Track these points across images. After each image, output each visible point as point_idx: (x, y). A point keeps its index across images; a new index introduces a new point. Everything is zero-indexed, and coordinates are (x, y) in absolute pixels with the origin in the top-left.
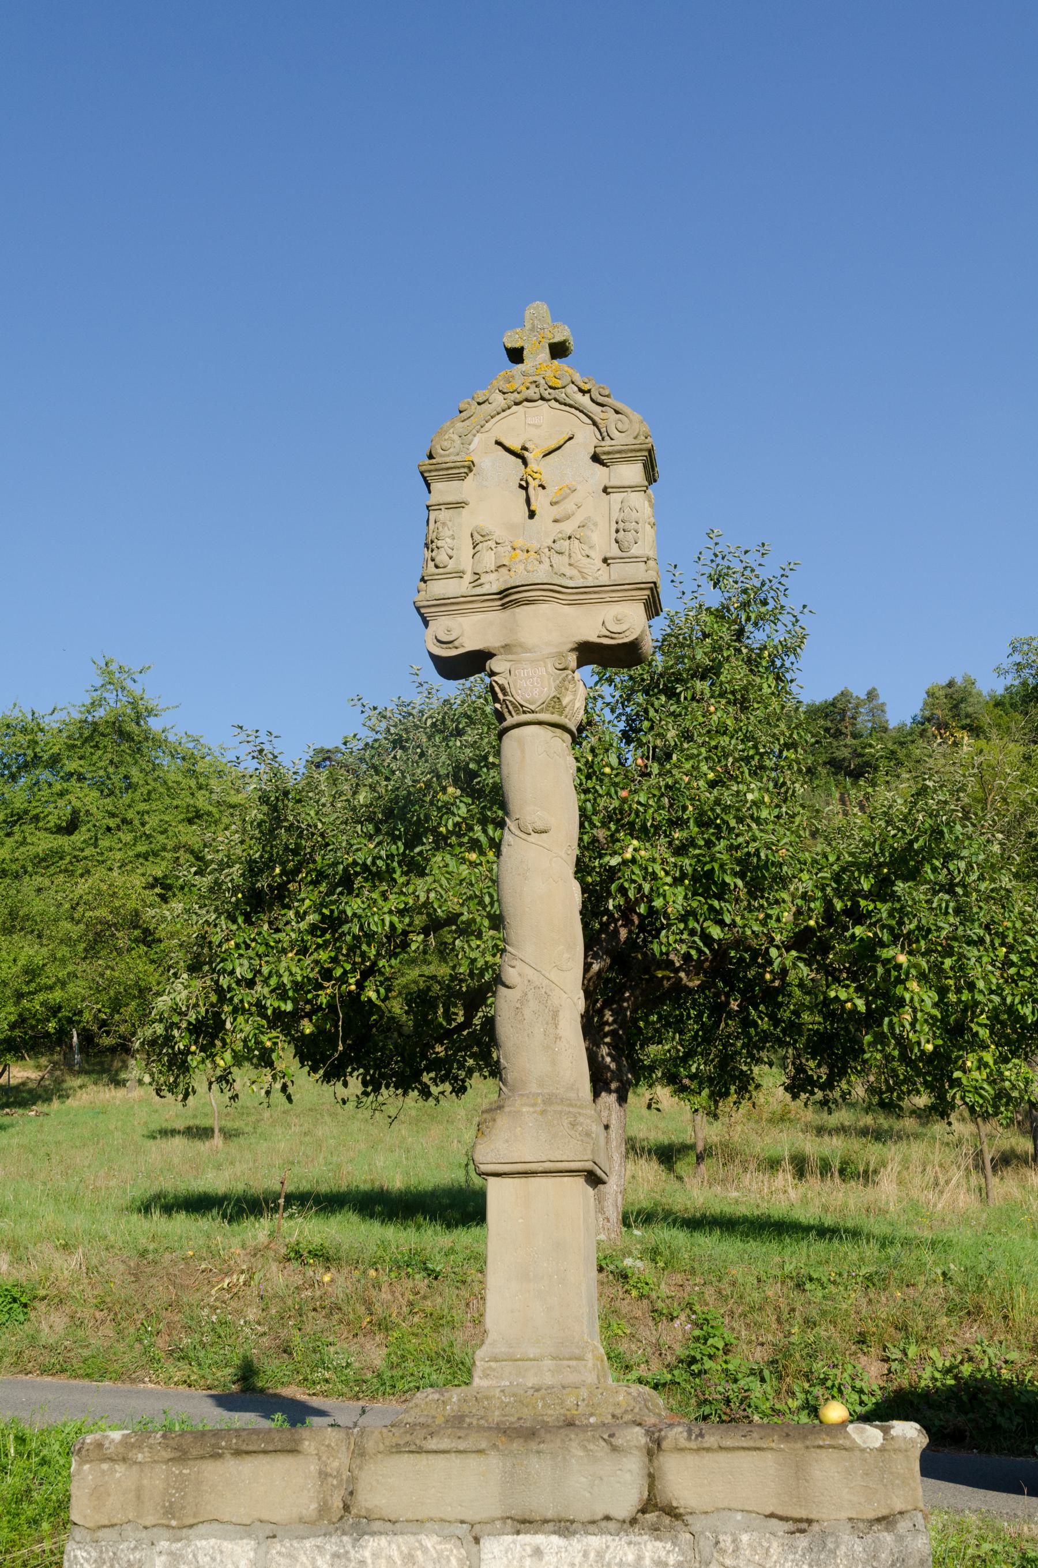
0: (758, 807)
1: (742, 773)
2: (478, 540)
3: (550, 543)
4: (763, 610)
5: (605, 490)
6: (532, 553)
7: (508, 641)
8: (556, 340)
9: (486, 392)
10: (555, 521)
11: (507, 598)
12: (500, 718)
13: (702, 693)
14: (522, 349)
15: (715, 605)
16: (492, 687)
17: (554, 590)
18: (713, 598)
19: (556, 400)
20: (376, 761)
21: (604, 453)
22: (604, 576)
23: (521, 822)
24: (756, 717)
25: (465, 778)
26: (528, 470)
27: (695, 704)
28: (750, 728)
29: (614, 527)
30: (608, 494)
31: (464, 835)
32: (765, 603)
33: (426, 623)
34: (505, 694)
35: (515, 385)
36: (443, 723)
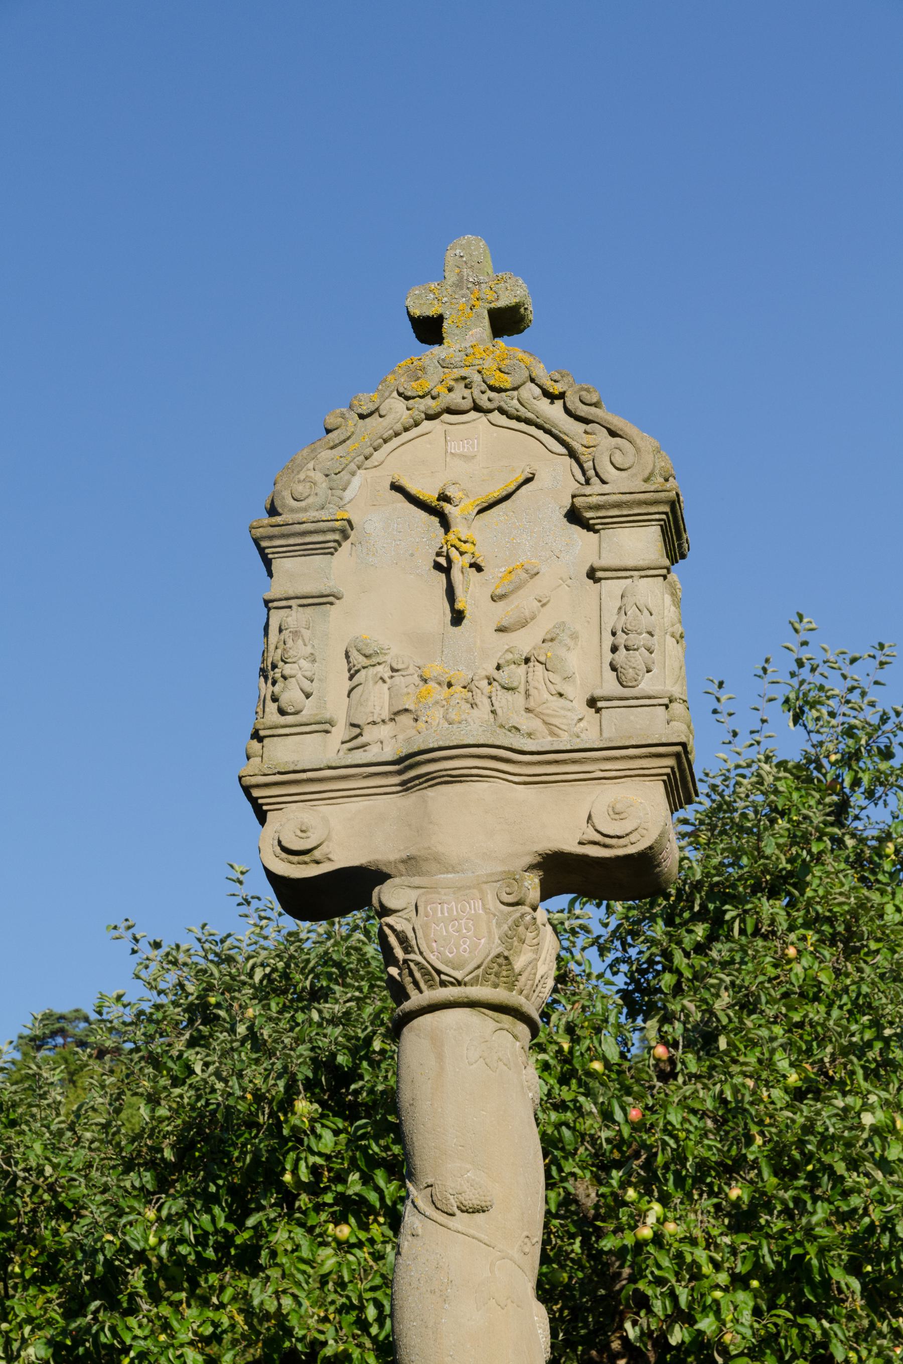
0: (884, 1139)
1: (852, 1073)
2: (358, 664)
3: (491, 670)
4: (884, 766)
5: (592, 574)
6: (457, 688)
7: (412, 851)
8: (501, 303)
9: (375, 396)
10: (501, 630)
11: (413, 770)
12: (398, 994)
13: (773, 922)
14: (440, 318)
15: (795, 757)
16: (383, 937)
17: (498, 758)
18: (792, 744)
19: (502, 411)
20: (157, 1047)
21: (591, 508)
22: (589, 731)
23: (436, 1190)
24: (875, 967)
25: (333, 1084)
26: (451, 537)
27: (760, 943)
28: (865, 989)
29: (608, 641)
30: (597, 580)
31: (327, 1189)
32: (887, 754)
33: (262, 816)
34: (407, 949)
35: (428, 383)
36: (286, 976)
